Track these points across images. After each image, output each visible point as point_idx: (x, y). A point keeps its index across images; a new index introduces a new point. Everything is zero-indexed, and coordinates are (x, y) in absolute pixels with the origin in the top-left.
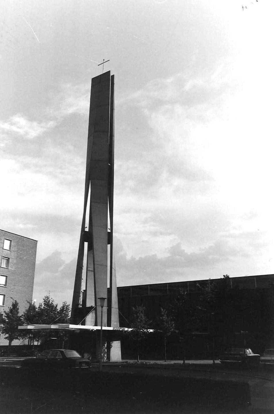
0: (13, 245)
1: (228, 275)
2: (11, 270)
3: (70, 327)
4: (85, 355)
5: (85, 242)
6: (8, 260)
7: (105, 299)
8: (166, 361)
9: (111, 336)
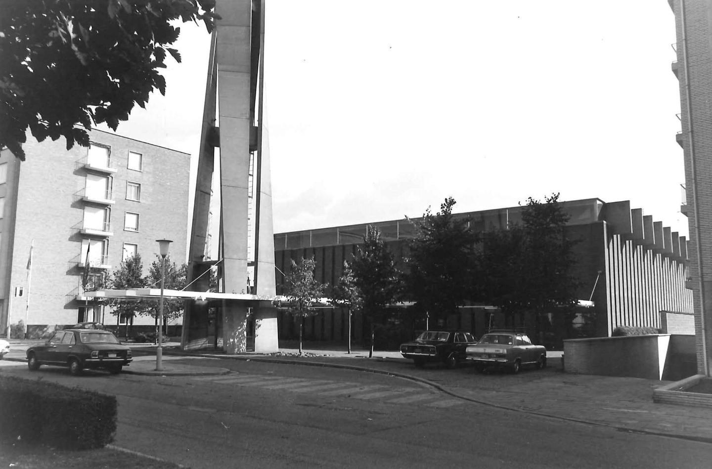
0: (145, 162)
1: (452, 198)
2: (144, 203)
3: (151, 294)
4: (219, 341)
5: (215, 148)
6: (139, 186)
7: (170, 243)
8: (350, 352)
9: (259, 309)
